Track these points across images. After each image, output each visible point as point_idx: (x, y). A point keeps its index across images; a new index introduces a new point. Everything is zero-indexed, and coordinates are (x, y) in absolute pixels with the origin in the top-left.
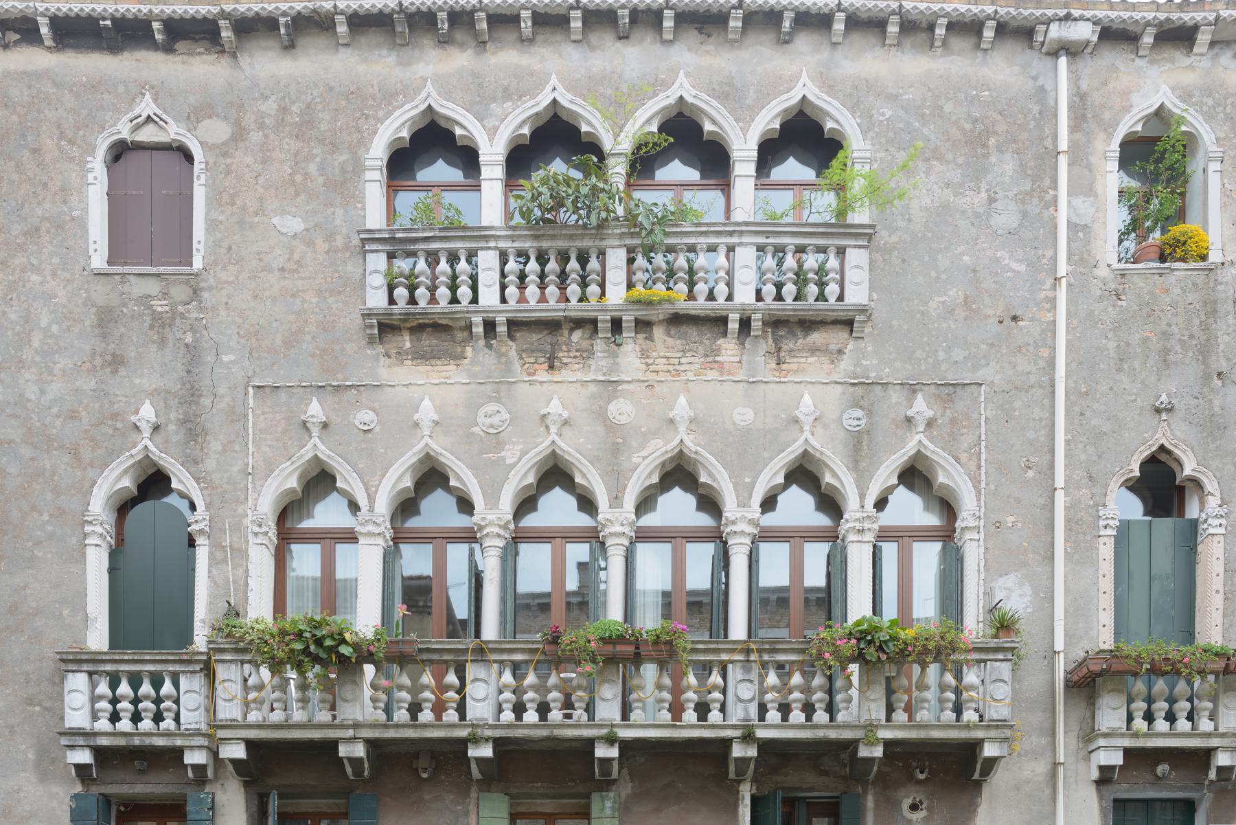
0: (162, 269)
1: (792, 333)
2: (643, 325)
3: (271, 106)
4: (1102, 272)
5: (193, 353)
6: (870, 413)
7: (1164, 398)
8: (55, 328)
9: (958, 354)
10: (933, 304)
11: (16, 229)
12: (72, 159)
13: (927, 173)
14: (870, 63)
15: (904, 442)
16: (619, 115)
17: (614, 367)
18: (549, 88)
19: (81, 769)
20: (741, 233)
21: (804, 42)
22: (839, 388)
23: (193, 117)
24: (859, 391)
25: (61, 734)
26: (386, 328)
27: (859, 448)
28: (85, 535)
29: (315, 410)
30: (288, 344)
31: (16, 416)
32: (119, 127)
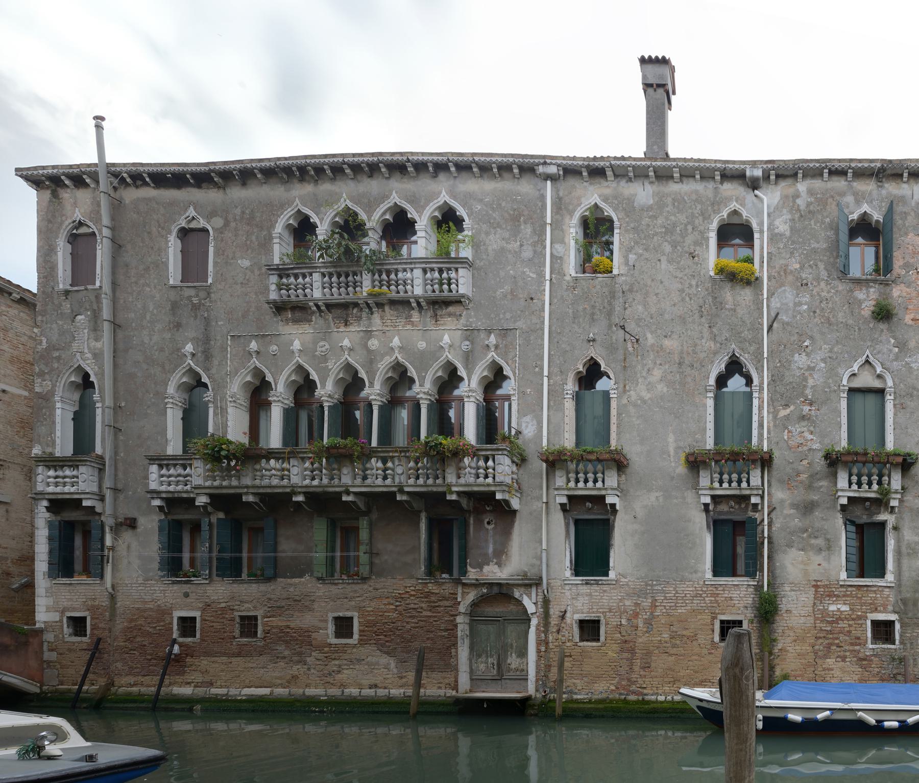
0: (195, 284)
1: (440, 307)
2: (380, 305)
3: (238, 211)
4: (568, 278)
5: (207, 321)
6: (472, 343)
7: (591, 335)
8: (155, 311)
9: (508, 316)
10: (498, 293)
11: (141, 267)
12: (162, 236)
13: (495, 234)
14: (470, 185)
15: (486, 355)
16: (370, 208)
17: (370, 325)
18: (342, 200)
19: (161, 508)
20: (415, 263)
21: (442, 176)
22: (460, 332)
23: (209, 217)
24: (468, 333)
25: (148, 492)
26: (280, 308)
27: (469, 358)
28: (166, 404)
29: (254, 345)
30: (243, 317)
31: (140, 350)
32: (181, 222)
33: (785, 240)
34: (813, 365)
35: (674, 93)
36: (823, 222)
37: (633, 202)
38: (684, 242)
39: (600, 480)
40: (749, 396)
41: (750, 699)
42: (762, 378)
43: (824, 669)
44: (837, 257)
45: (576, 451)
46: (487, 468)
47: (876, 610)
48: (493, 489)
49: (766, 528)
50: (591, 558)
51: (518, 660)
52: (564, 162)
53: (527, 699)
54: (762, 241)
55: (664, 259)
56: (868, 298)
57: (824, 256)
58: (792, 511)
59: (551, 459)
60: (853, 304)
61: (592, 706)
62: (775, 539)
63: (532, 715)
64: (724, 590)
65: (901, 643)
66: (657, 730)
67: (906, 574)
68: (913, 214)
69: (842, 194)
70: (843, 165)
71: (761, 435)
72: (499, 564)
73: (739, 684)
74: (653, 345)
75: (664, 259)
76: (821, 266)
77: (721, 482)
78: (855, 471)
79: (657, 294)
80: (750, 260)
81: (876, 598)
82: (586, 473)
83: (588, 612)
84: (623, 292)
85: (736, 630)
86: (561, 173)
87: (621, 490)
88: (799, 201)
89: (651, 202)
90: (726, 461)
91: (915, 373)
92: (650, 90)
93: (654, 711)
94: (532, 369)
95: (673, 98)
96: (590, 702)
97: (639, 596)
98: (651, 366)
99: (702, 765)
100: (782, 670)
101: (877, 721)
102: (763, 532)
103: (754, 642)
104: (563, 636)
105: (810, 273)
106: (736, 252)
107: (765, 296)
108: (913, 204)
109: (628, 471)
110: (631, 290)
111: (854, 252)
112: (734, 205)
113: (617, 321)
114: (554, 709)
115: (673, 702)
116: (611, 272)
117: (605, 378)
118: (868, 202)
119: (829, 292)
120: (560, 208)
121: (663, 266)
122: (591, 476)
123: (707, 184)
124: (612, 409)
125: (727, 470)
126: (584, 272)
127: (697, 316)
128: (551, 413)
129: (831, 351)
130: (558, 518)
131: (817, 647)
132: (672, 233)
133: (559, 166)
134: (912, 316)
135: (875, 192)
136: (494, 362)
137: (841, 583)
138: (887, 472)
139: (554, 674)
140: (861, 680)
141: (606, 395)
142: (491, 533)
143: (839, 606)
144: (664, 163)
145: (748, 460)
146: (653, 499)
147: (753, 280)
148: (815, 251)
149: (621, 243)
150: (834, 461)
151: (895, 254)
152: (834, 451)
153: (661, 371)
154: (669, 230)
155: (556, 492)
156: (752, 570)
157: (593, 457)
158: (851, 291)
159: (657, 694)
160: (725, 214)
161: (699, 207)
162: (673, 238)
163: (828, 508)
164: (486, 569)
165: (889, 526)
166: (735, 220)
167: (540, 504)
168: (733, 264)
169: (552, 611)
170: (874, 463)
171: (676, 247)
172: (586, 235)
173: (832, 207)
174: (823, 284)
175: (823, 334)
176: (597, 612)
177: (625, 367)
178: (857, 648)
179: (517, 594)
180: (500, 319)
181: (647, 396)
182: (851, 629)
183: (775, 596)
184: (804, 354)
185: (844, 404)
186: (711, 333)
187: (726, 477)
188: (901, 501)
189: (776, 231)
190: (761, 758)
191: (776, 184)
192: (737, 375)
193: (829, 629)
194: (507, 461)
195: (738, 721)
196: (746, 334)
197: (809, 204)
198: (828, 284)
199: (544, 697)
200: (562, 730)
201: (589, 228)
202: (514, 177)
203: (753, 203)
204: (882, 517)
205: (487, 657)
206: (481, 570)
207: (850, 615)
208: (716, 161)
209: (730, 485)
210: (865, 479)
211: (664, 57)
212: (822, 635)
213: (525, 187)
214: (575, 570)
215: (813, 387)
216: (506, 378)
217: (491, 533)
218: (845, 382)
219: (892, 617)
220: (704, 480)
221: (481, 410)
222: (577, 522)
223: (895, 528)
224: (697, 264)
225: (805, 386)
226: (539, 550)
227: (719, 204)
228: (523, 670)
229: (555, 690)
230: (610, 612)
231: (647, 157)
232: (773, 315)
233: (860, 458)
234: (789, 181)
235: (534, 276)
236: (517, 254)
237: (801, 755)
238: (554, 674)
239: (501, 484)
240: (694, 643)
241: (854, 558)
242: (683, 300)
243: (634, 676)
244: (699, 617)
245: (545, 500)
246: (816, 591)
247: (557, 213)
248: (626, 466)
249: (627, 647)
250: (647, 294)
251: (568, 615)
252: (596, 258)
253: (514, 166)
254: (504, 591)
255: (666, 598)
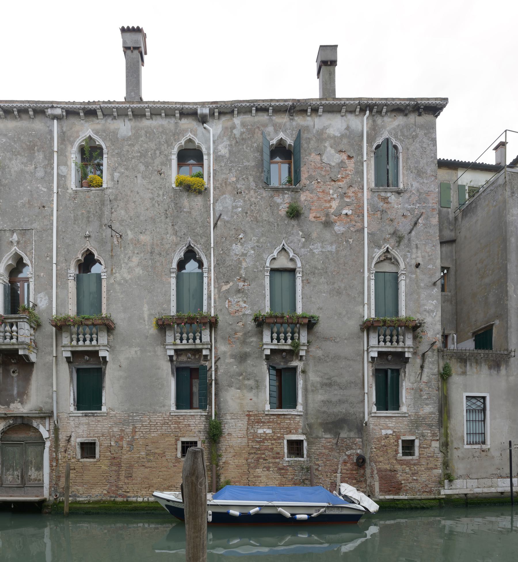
4: (70, 191)
7: (87, 233)
9: (26, 219)
10: (19, 203)
13: (16, 160)
15: (11, 249)
33: (225, 160)
34: (245, 252)
35: (146, 54)
36: (252, 147)
37: (117, 134)
38: (154, 163)
39: (95, 339)
40: (201, 275)
41: (203, 499)
42: (210, 262)
43: (255, 477)
44: (262, 172)
45: (77, 319)
46: (12, 332)
47: (290, 432)
48: (16, 347)
49: (213, 373)
50: (89, 396)
51: (36, 473)
52: (67, 106)
53: (43, 501)
54: (209, 161)
55: (139, 176)
56: (283, 201)
57: (253, 171)
58: (232, 360)
59: (59, 324)
60: (273, 206)
61: (91, 506)
62: (220, 381)
63: (46, 513)
64: (184, 419)
65: (308, 456)
66: (137, 523)
67: (311, 405)
68: (314, 139)
69: (265, 126)
70: (266, 104)
71: (209, 304)
72: (22, 402)
73: (195, 489)
74: (132, 239)
75: (139, 176)
76: (251, 179)
77: (181, 339)
78: (275, 330)
79: (134, 202)
80: (200, 176)
81: (290, 424)
82: (84, 335)
83: (87, 437)
84: (110, 201)
85: (193, 448)
86: (64, 114)
87: (110, 347)
88: (235, 131)
89: (130, 134)
90: (185, 324)
91: (317, 257)
92: (129, 52)
93: (135, 509)
94: (44, 258)
95: (145, 57)
96: (89, 503)
97: (123, 425)
98: (131, 255)
99: (169, 549)
100: (225, 478)
101: (292, 515)
102: (211, 376)
103: (205, 457)
104: (69, 454)
105: (243, 185)
106: (191, 170)
107: (212, 202)
108: (315, 132)
109: (115, 332)
110: (116, 199)
111: (274, 168)
112: (189, 135)
113: (106, 222)
114: (63, 508)
115: (148, 502)
116: (101, 186)
117: (98, 264)
118: (282, 131)
119: (256, 198)
120: (64, 140)
121: (139, 181)
122: (88, 336)
123: (170, 120)
124: (103, 287)
125: (185, 330)
126: (82, 187)
127: (163, 218)
128: (58, 291)
129: (258, 242)
130: (65, 367)
131: (249, 460)
132: (145, 157)
133: (62, 108)
134: (314, 215)
135: (288, 124)
136: (16, 254)
137: (266, 413)
138: (297, 331)
139: (62, 483)
140: (281, 485)
141: (99, 276)
142: (15, 379)
143: (265, 430)
144: (139, 105)
145: (200, 323)
146: (133, 352)
147: (203, 190)
148: (246, 168)
149: (108, 165)
150: (260, 322)
151: (302, 169)
152: (260, 315)
153: (138, 259)
154: (143, 155)
155: (63, 349)
156: (204, 404)
157: (89, 323)
158: (272, 197)
159: (137, 496)
160: (183, 142)
161: (164, 137)
162: (146, 160)
163: (256, 358)
164: (12, 406)
165: (299, 370)
166: (190, 146)
167: (51, 358)
168: (189, 179)
169: (60, 437)
170: (288, 324)
171: (148, 167)
172: (83, 159)
173: (258, 135)
174: (252, 192)
175: (252, 229)
176: (94, 437)
177: (112, 256)
178: (277, 460)
179: (35, 424)
180: (20, 222)
181: (128, 277)
182: (273, 446)
183: (220, 423)
184: (239, 244)
185: (267, 280)
186: (174, 229)
187: (185, 335)
188: (307, 351)
189: (219, 154)
190: (211, 543)
191: (219, 119)
192: (192, 261)
193: (258, 447)
194: (27, 326)
195: (196, 516)
196: (198, 230)
197: (242, 133)
198: (256, 192)
199: (55, 499)
200: (69, 523)
201: (85, 154)
202: (30, 117)
203: (203, 133)
204: (294, 363)
205: (14, 471)
206: (9, 407)
207: (273, 436)
208: (176, 103)
209: (188, 342)
210: (282, 335)
211: (138, 27)
212: (253, 451)
213: (39, 125)
214: (77, 406)
215: (245, 268)
216: (25, 265)
217: (15, 379)
218: (268, 264)
219: (302, 437)
220: (170, 338)
221: (7, 289)
222: (78, 371)
223: (303, 372)
224: (163, 179)
225: (240, 268)
226: (51, 391)
227: (178, 135)
228: (40, 480)
229: (63, 495)
230: (103, 436)
231: (127, 101)
232: (218, 216)
233: (279, 320)
234: (228, 117)
235: (45, 190)
236: (32, 174)
237: (239, 540)
238: (62, 483)
239: (22, 343)
240: (163, 458)
241: (275, 394)
242: (153, 205)
243: (120, 483)
244: (167, 439)
245: (55, 355)
246: (249, 419)
247: (62, 143)
248: (113, 329)
249: (115, 462)
250: (127, 202)
251: (72, 439)
252: (90, 176)
253: (30, 109)
254: (26, 421)
255: (143, 425)
